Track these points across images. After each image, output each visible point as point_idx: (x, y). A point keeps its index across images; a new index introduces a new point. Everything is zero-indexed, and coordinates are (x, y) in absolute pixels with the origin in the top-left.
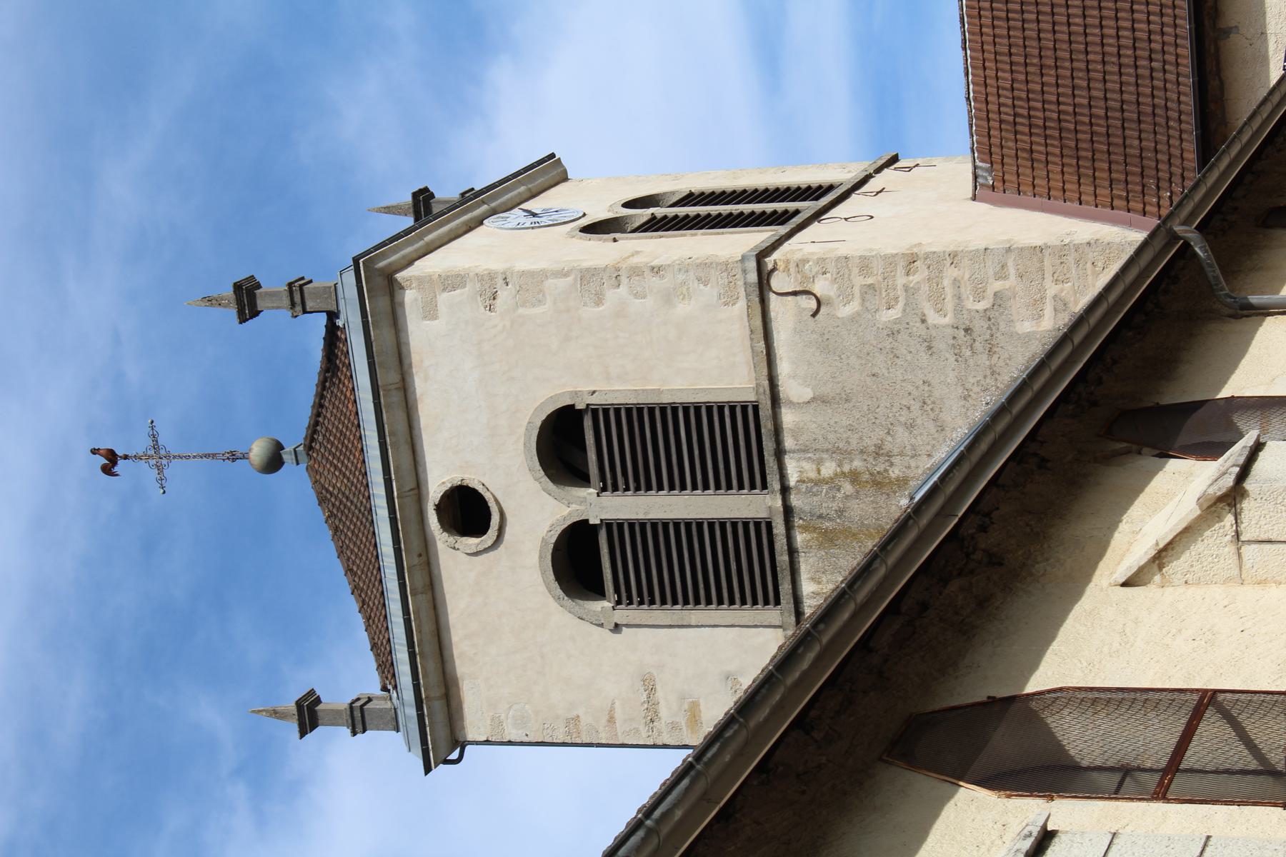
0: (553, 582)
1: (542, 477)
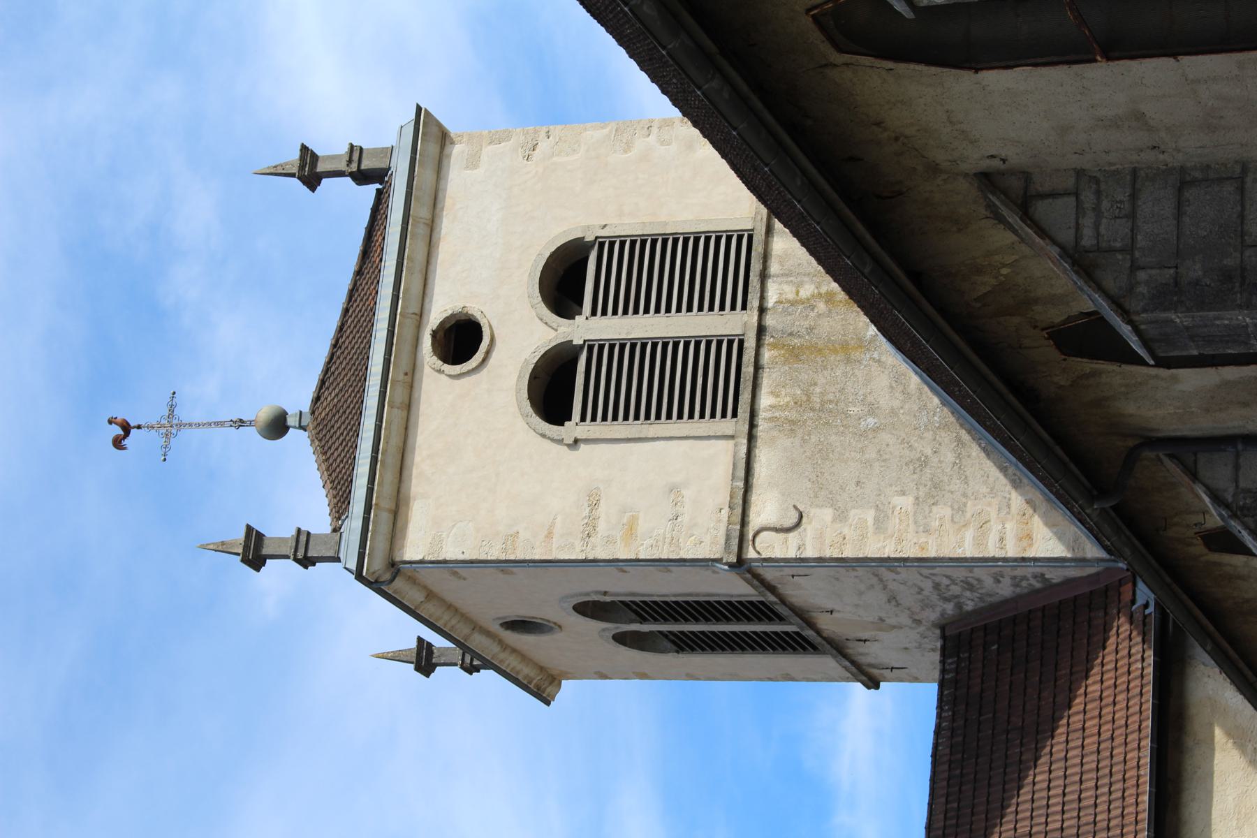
0: (525, 400)
1: (538, 303)
